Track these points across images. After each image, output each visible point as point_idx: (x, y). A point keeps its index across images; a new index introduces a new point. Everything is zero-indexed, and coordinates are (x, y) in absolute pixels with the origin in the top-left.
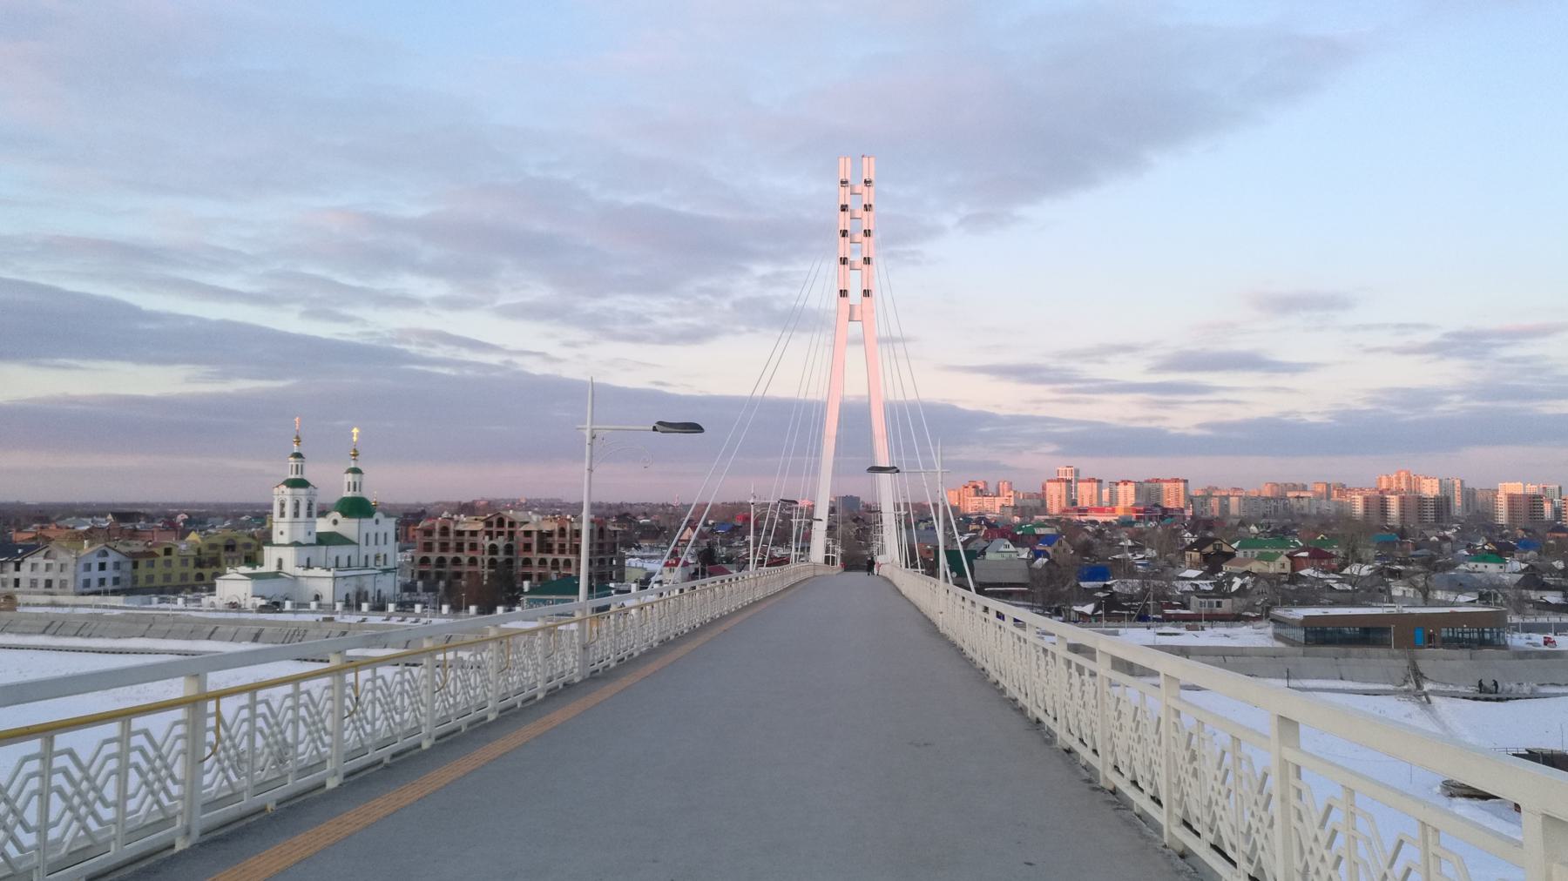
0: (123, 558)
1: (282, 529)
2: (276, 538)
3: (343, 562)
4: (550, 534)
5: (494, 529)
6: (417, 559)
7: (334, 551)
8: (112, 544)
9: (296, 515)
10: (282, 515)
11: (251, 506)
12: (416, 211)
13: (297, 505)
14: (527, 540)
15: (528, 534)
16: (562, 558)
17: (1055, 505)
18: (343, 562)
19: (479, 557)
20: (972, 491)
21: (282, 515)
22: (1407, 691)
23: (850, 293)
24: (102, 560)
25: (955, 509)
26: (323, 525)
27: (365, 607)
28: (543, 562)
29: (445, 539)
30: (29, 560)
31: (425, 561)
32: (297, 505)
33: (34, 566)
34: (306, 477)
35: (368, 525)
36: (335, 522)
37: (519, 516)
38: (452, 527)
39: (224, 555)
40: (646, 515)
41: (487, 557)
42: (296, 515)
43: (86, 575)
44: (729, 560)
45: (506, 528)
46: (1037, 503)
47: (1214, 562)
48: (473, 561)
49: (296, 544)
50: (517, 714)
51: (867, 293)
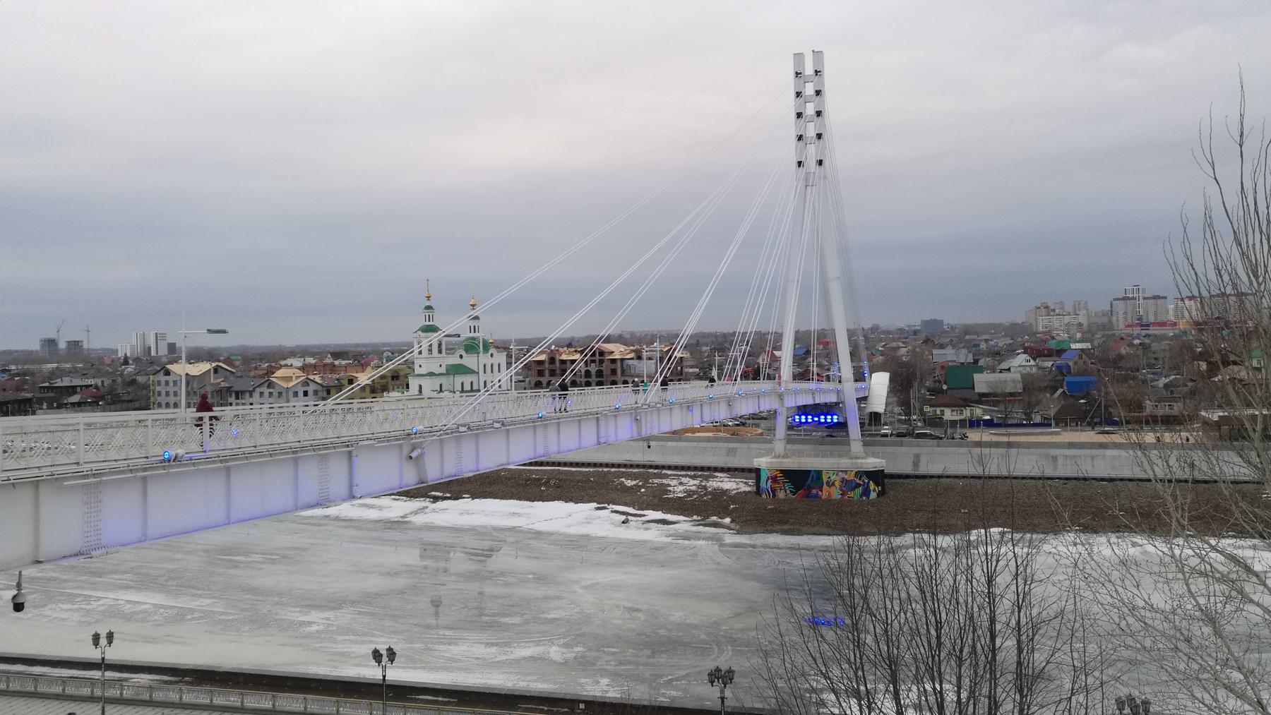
0: (319, 388)
1: (424, 365)
2: (418, 371)
3: (467, 387)
7: (459, 380)
8: (311, 377)
11: (389, 345)
12: (1057, 554)
14: (613, 366)
15: (614, 361)
17: (1120, 322)
18: (467, 387)
20: (1044, 311)
24: (305, 389)
25: (410, 364)
26: (454, 360)
29: (552, 367)
30: (258, 390)
33: (262, 394)
34: (436, 323)
35: (485, 359)
36: (461, 357)
38: (558, 358)
39: (391, 383)
40: (15, 362)
44: (840, 551)
45: (597, 357)
46: (1105, 320)
49: (431, 374)
51: (820, 163)
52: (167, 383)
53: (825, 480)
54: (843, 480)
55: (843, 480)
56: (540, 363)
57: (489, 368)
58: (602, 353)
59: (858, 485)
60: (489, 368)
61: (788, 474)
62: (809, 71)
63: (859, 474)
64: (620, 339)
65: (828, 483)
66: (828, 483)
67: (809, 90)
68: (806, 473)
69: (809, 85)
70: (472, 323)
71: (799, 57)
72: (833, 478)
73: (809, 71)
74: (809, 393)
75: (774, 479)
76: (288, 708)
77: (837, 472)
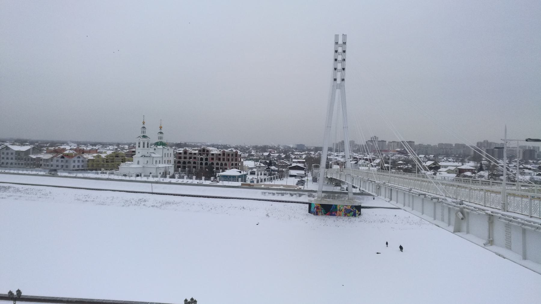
4: (220, 155)
5: (202, 152)
6: (177, 162)
9: (144, 147)
10: (139, 147)
13: (144, 143)
15: (213, 154)
16: (224, 163)
19: (196, 162)
21: (139, 147)
22: (228, 148)
23: (337, 80)
27: (168, 176)
28: (217, 164)
31: (179, 162)
32: (144, 143)
37: (211, 148)
41: (199, 162)
42: (144, 147)
43: (67, 164)
47: (430, 168)
48: (195, 163)
50: (460, 153)
51: (343, 80)
52: (8, 154)
53: (338, 208)
54: (345, 209)
55: (345, 209)
56: (180, 153)
57: (167, 155)
58: (208, 151)
59: (351, 211)
60: (167, 155)
61: (323, 206)
62: (340, 42)
63: (352, 207)
64: (213, 146)
65: (339, 210)
66: (339, 210)
67: (340, 50)
68: (330, 206)
69: (340, 48)
70: (160, 135)
71: (337, 36)
72: (342, 208)
73: (340, 42)
74: (204, 160)
75: (317, 208)
76: (14, 170)
77: (343, 206)
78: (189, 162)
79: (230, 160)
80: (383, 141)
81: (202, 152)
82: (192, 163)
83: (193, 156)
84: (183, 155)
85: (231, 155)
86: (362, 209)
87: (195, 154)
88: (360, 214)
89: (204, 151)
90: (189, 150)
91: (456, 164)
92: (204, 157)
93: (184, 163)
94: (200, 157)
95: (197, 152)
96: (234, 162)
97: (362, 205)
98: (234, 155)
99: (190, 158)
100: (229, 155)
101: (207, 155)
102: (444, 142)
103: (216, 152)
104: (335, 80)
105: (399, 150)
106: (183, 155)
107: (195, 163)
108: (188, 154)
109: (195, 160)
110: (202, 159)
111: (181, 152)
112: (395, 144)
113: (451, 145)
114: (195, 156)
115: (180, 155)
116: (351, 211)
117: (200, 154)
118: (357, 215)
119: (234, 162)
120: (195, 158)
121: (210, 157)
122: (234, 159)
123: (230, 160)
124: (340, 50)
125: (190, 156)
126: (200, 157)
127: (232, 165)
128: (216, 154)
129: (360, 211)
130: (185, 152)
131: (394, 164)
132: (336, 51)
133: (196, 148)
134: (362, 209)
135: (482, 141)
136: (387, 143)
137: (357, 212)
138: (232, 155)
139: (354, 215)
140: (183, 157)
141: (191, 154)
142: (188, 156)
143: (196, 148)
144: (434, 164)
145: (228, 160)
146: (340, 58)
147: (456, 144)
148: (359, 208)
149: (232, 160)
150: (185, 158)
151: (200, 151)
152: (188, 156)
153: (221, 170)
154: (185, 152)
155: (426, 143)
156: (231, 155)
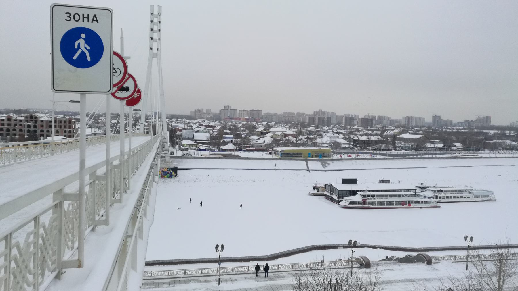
4: (51, 122)
5: (29, 119)
15: (42, 121)
23: (154, 49)
41: (26, 129)
48: (21, 130)
51: (159, 49)
56: (3, 120)
58: (36, 118)
59: (168, 173)
62: (156, 13)
63: (168, 169)
71: (152, 7)
73: (156, 13)
78: (14, 130)
79: (63, 127)
80: (234, 110)
81: (29, 119)
82: (18, 130)
83: (19, 123)
84: (6, 122)
85: (63, 122)
86: (178, 171)
87: (21, 121)
88: (176, 176)
89: (31, 117)
90: (14, 116)
91: (284, 130)
92: (32, 123)
93: (8, 130)
94: (26, 124)
95: (23, 118)
96: (67, 130)
97: (179, 167)
98: (67, 123)
99: (16, 125)
100: (61, 122)
101: (36, 122)
102: (288, 111)
103: (47, 119)
104: (151, 49)
105: (247, 118)
106: (6, 122)
107: (21, 130)
108: (12, 121)
109: (21, 128)
110: (29, 126)
111: (4, 118)
112: (245, 113)
113: (294, 114)
114: (21, 123)
115: (3, 122)
116: (168, 173)
117: (27, 121)
118: (173, 176)
119: (67, 130)
120: (21, 125)
121: (38, 124)
122: (67, 126)
123: (63, 127)
124: (156, 20)
125: (15, 122)
126: (26, 124)
127: (65, 132)
128: (47, 121)
129: (176, 172)
130: (9, 119)
131: (364, 145)
132: (152, 21)
133: (22, 115)
134: (178, 171)
135: (318, 110)
136: (238, 112)
137: (173, 173)
138: (65, 122)
139: (171, 176)
140: (6, 124)
141: (16, 120)
142: (12, 123)
143: (22, 115)
144: (265, 130)
145: (61, 127)
146: (155, 28)
147: (297, 113)
148: (175, 170)
149: (65, 127)
150: (9, 125)
151: (27, 117)
152: (12, 123)
153: (42, 138)
154: (9, 119)
155: (272, 112)
156: (63, 122)
